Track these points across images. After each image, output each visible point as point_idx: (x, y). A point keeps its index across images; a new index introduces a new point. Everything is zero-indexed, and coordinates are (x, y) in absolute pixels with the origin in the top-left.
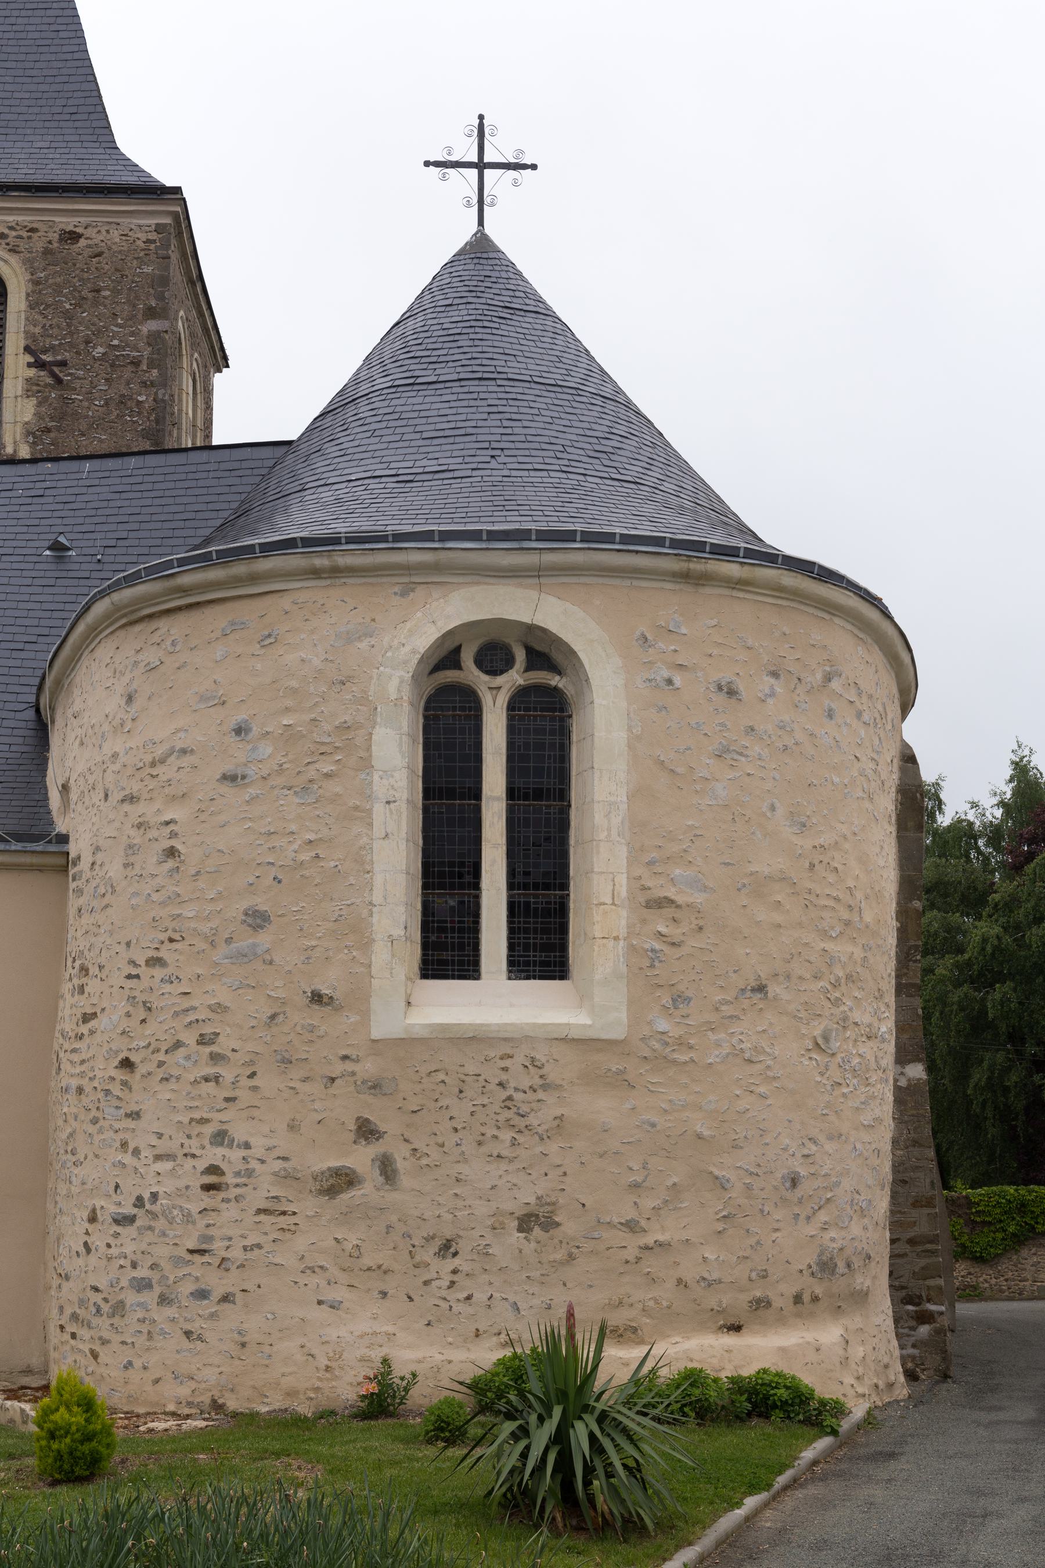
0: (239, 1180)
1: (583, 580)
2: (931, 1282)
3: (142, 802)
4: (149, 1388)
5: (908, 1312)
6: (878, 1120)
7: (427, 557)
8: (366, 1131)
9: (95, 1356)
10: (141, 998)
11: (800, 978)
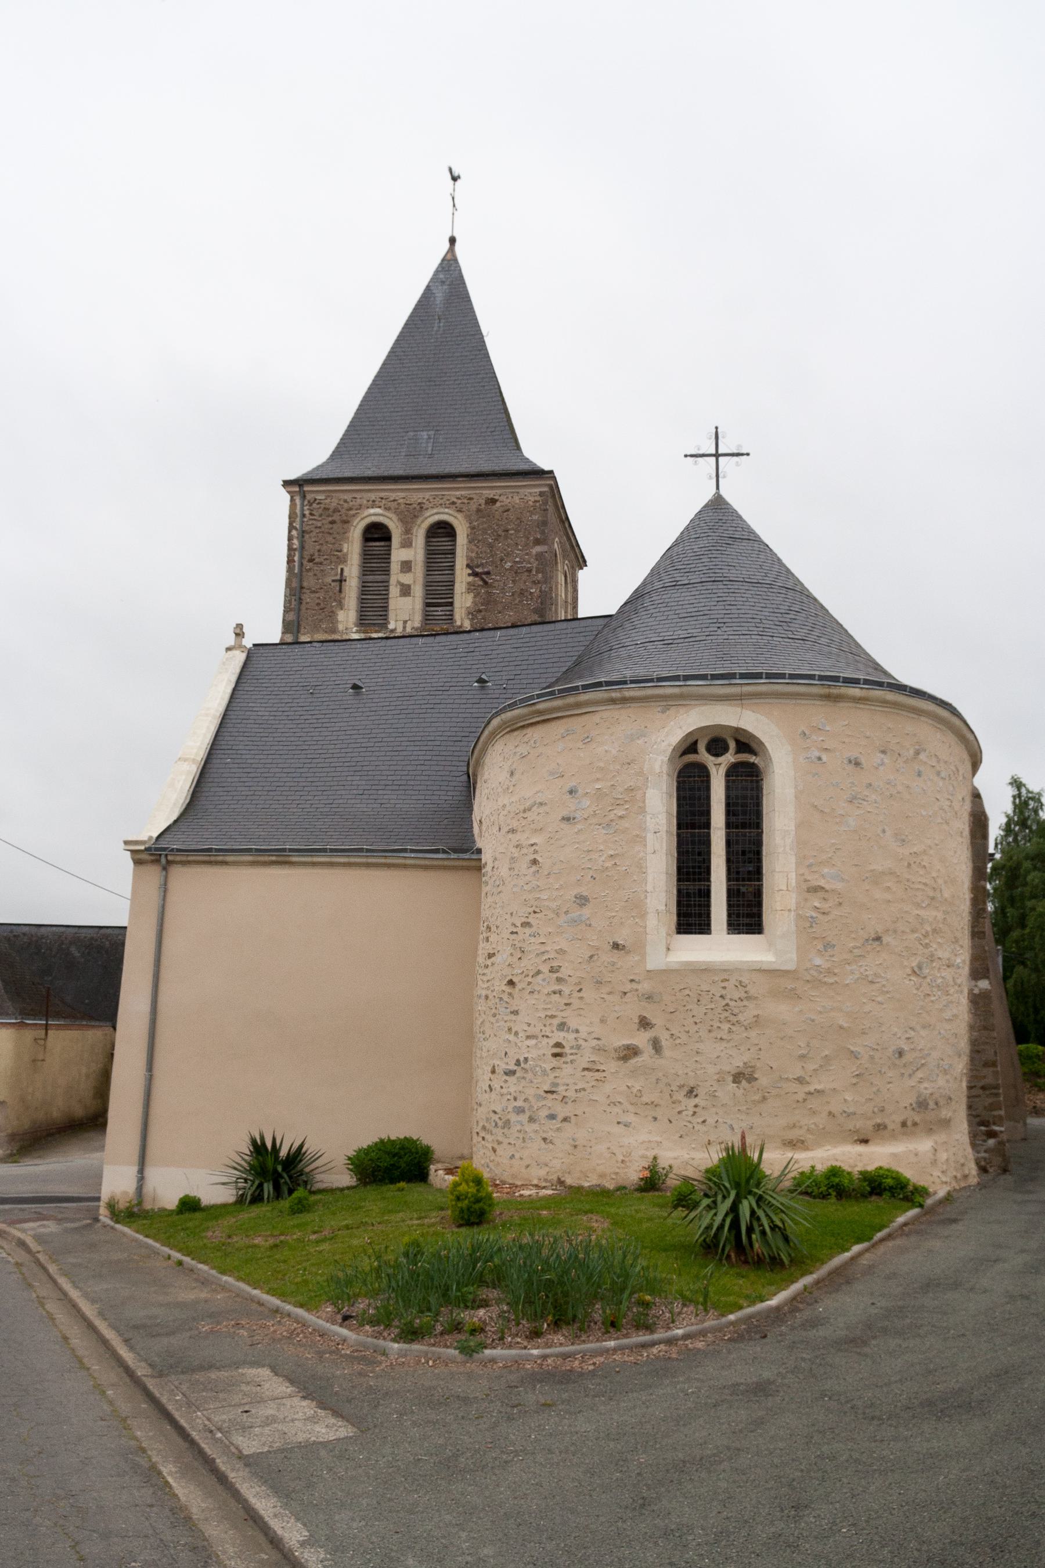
0: (573, 1051)
1: (767, 700)
2: (996, 1113)
3: (518, 833)
4: (523, 1170)
5: (981, 1131)
6: (955, 1016)
7: (676, 690)
8: (644, 1023)
9: (494, 1150)
10: (518, 945)
11: (903, 932)
